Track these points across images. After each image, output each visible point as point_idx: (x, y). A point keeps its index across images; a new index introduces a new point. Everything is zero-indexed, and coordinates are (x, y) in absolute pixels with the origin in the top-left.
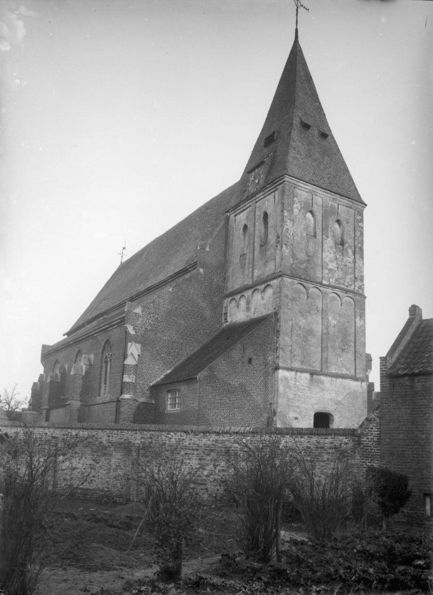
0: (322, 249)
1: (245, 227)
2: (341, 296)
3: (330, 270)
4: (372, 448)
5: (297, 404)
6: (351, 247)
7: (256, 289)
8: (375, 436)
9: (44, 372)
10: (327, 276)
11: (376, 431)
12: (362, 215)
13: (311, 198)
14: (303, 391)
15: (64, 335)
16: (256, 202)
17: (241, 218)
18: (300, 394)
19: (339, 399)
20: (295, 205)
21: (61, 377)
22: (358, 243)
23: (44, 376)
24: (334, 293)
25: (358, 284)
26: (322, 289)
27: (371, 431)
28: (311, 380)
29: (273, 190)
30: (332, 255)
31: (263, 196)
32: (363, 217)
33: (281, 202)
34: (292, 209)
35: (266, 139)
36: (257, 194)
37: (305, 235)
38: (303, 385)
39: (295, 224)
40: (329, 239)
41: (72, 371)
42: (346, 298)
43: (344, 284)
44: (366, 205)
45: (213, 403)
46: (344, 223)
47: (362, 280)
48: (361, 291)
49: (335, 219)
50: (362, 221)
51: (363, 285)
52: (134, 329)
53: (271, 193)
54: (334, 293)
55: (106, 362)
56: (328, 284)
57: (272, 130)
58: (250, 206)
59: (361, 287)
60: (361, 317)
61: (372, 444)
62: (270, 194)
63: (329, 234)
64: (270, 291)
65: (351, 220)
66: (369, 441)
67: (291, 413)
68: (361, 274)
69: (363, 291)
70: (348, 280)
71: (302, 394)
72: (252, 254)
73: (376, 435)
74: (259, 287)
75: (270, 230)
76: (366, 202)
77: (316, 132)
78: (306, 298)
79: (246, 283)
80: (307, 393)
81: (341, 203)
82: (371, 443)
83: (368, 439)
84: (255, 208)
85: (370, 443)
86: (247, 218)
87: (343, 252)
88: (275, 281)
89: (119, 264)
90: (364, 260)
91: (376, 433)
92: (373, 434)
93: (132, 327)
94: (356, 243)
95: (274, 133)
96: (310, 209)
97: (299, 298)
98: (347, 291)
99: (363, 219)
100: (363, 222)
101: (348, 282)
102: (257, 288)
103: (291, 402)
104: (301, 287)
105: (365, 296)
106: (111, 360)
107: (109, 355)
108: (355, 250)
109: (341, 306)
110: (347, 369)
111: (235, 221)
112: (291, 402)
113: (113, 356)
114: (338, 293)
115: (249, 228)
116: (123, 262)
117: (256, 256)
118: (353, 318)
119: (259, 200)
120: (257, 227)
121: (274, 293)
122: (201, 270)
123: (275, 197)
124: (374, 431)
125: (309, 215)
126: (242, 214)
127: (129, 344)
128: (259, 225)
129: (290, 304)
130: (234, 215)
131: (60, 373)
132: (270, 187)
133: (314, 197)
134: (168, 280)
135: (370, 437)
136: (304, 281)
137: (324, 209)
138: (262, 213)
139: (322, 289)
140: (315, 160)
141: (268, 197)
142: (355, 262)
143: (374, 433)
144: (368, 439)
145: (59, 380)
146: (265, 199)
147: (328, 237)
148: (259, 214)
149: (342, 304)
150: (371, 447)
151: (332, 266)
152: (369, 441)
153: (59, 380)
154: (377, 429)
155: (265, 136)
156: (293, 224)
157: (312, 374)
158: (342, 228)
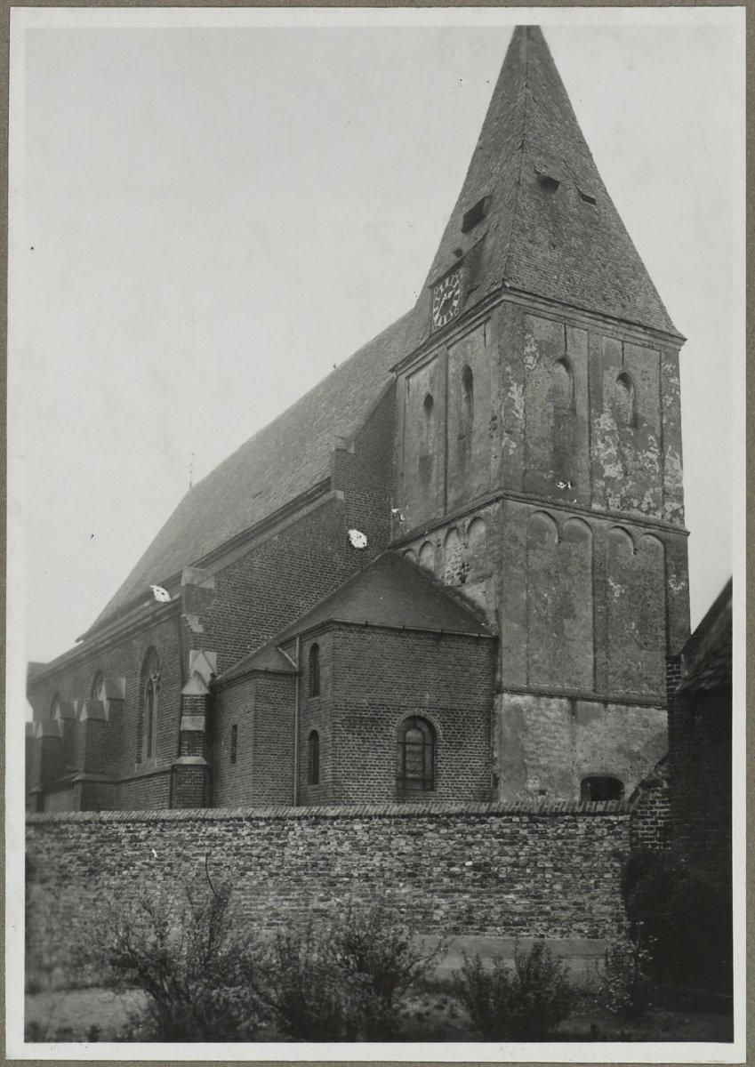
0: (590, 438)
1: (429, 401)
2: (634, 534)
3: (608, 479)
4: (655, 841)
5: (543, 761)
6: (653, 429)
7: (453, 528)
8: (659, 818)
9: (34, 719)
10: (601, 493)
11: (662, 808)
12: (676, 362)
13: (563, 332)
14: (556, 734)
15: (77, 641)
16: (448, 348)
17: (421, 381)
18: (549, 741)
19: (636, 748)
20: (528, 350)
21: (65, 725)
22: (669, 420)
23: (34, 726)
24: (618, 527)
25: (670, 506)
26: (591, 520)
27: (652, 808)
28: (573, 712)
29: (481, 321)
30: (613, 450)
31: (462, 334)
32: (678, 365)
33: (496, 345)
34: (522, 357)
35: (466, 216)
36: (451, 330)
37: (551, 410)
38: (554, 723)
39: (529, 387)
40: (604, 416)
41: (82, 715)
42: (645, 537)
43: (639, 508)
44: (685, 340)
45: (364, 766)
46: (638, 380)
47: (680, 498)
48: (677, 522)
49: (616, 374)
50: (676, 373)
51: (683, 507)
52: (201, 621)
53: (478, 327)
54: (618, 527)
55: (150, 692)
56: (603, 509)
57: (485, 190)
58: (437, 356)
59: (678, 514)
60: (678, 573)
61: (656, 834)
62: (474, 329)
63: (605, 404)
64: (481, 529)
65: (653, 374)
66: (649, 829)
67: (531, 781)
68: (678, 485)
69: (682, 521)
70: (648, 499)
71: (553, 741)
72: (442, 456)
73: (662, 815)
74: (459, 523)
75: (477, 404)
76: (685, 336)
77: (572, 193)
78: (556, 541)
79: (433, 515)
80: (563, 738)
81: (628, 339)
82: (652, 832)
83: (646, 823)
84: (447, 361)
85: (650, 832)
86: (432, 380)
87: (639, 444)
88: (489, 509)
89: (186, 489)
90: (684, 454)
91: (662, 810)
92: (655, 813)
93: (197, 618)
94: (665, 421)
95: (482, 202)
96: (560, 354)
97: (541, 542)
98: (647, 524)
99: (678, 369)
100: (678, 376)
101: (649, 504)
102: (453, 525)
103: (531, 759)
104: (547, 520)
105: (686, 532)
106: (158, 688)
107: (155, 677)
108: (662, 434)
109: (635, 554)
110: (651, 686)
111: (408, 389)
112: (531, 759)
113: (163, 679)
114: (627, 527)
115: (435, 402)
116: (194, 483)
117: (450, 458)
118: (662, 577)
119: (454, 343)
120: (451, 400)
121: (490, 533)
122: (340, 495)
123: (485, 335)
124: (656, 808)
125: (561, 369)
126: (423, 372)
127: (192, 653)
128: (456, 391)
129: (522, 555)
130: (406, 375)
131: (61, 718)
132: (475, 315)
133: (569, 331)
134: (275, 518)
135: (649, 820)
136: (552, 506)
137: (591, 353)
138: (461, 368)
139: (591, 520)
140: (568, 252)
141: (473, 334)
142: (662, 461)
143: (658, 811)
144: (646, 823)
145: (61, 734)
146: (466, 339)
147: (602, 412)
148: (454, 368)
149: (635, 550)
150: (653, 839)
151: (612, 471)
152: (649, 829)
153: (61, 734)
154: (663, 802)
155: (465, 210)
156: (523, 390)
157: (573, 699)
158: (632, 392)
